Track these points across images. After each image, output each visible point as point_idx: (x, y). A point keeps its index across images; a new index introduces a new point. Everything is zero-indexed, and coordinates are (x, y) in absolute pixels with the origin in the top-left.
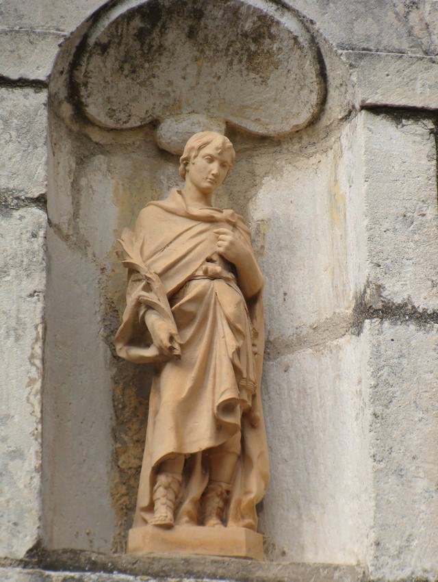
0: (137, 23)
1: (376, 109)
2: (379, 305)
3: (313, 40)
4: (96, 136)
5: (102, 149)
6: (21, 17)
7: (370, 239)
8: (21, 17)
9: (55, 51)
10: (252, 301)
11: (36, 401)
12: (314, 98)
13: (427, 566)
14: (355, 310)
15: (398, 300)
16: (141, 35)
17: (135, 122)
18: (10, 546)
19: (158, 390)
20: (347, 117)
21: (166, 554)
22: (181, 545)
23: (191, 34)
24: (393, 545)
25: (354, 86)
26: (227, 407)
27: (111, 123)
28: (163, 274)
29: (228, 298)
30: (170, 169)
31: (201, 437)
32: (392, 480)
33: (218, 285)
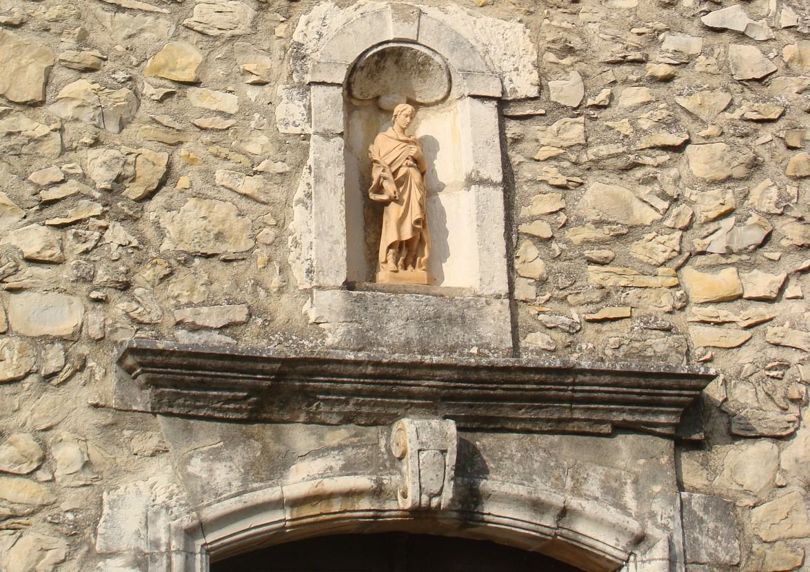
0: (376, 58)
1: (474, 97)
2: (478, 179)
3: (447, 67)
4: (355, 103)
5: (357, 108)
6: (331, 56)
7: (474, 151)
8: (331, 56)
9: (345, 71)
10: (423, 174)
11: (344, 219)
12: (446, 90)
13: (501, 289)
14: (466, 180)
15: (485, 177)
16: (377, 63)
17: (370, 97)
18: (336, 281)
19: (387, 213)
20: (461, 98)
21: (396, 283)
22: (401, 279)
23: (397, 62)
24: (487, 280)
25: (461, 86)
26: (417, 222)
27: (361, 97)
28: (390, 165)
29: (415, 176)
30: (383, 116)
31: (407, 234)
32: (486, 253)
33: (411, 169)
